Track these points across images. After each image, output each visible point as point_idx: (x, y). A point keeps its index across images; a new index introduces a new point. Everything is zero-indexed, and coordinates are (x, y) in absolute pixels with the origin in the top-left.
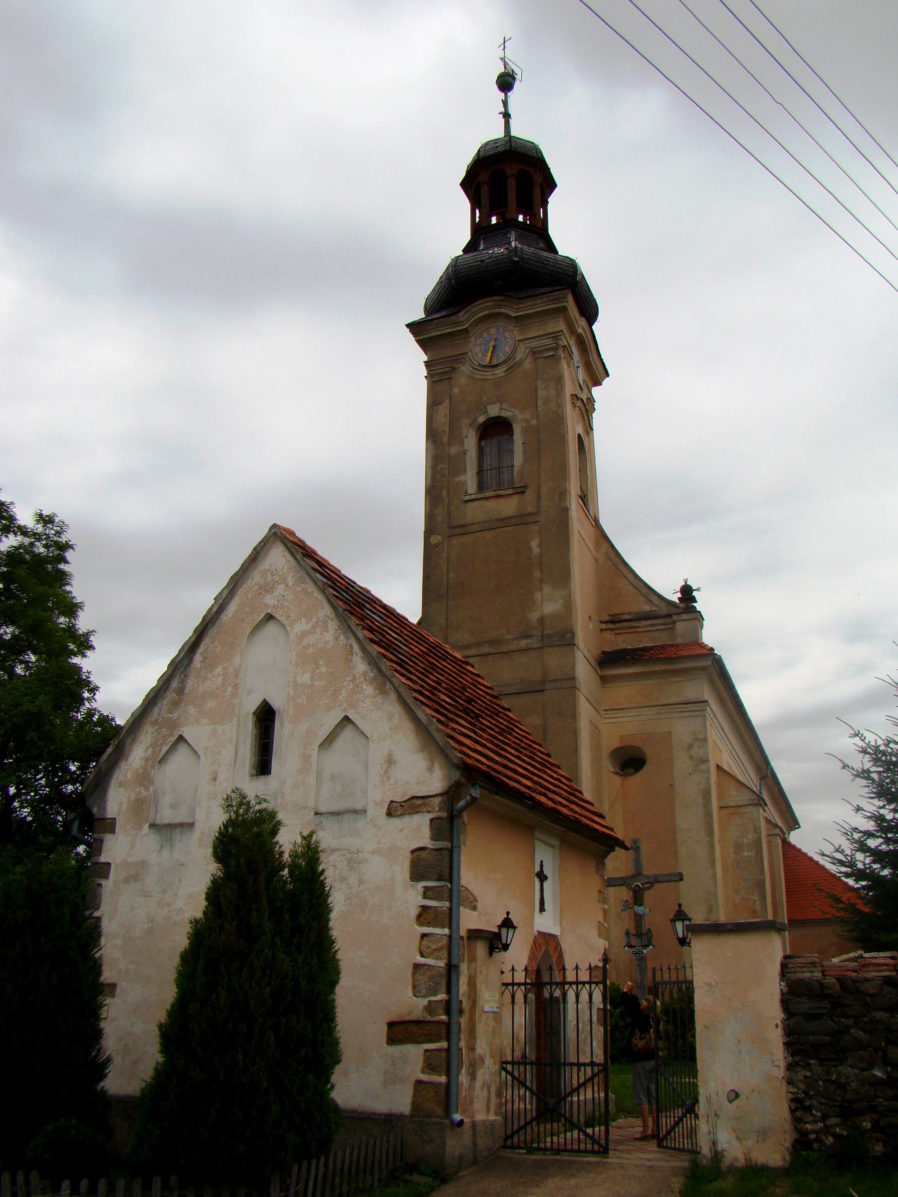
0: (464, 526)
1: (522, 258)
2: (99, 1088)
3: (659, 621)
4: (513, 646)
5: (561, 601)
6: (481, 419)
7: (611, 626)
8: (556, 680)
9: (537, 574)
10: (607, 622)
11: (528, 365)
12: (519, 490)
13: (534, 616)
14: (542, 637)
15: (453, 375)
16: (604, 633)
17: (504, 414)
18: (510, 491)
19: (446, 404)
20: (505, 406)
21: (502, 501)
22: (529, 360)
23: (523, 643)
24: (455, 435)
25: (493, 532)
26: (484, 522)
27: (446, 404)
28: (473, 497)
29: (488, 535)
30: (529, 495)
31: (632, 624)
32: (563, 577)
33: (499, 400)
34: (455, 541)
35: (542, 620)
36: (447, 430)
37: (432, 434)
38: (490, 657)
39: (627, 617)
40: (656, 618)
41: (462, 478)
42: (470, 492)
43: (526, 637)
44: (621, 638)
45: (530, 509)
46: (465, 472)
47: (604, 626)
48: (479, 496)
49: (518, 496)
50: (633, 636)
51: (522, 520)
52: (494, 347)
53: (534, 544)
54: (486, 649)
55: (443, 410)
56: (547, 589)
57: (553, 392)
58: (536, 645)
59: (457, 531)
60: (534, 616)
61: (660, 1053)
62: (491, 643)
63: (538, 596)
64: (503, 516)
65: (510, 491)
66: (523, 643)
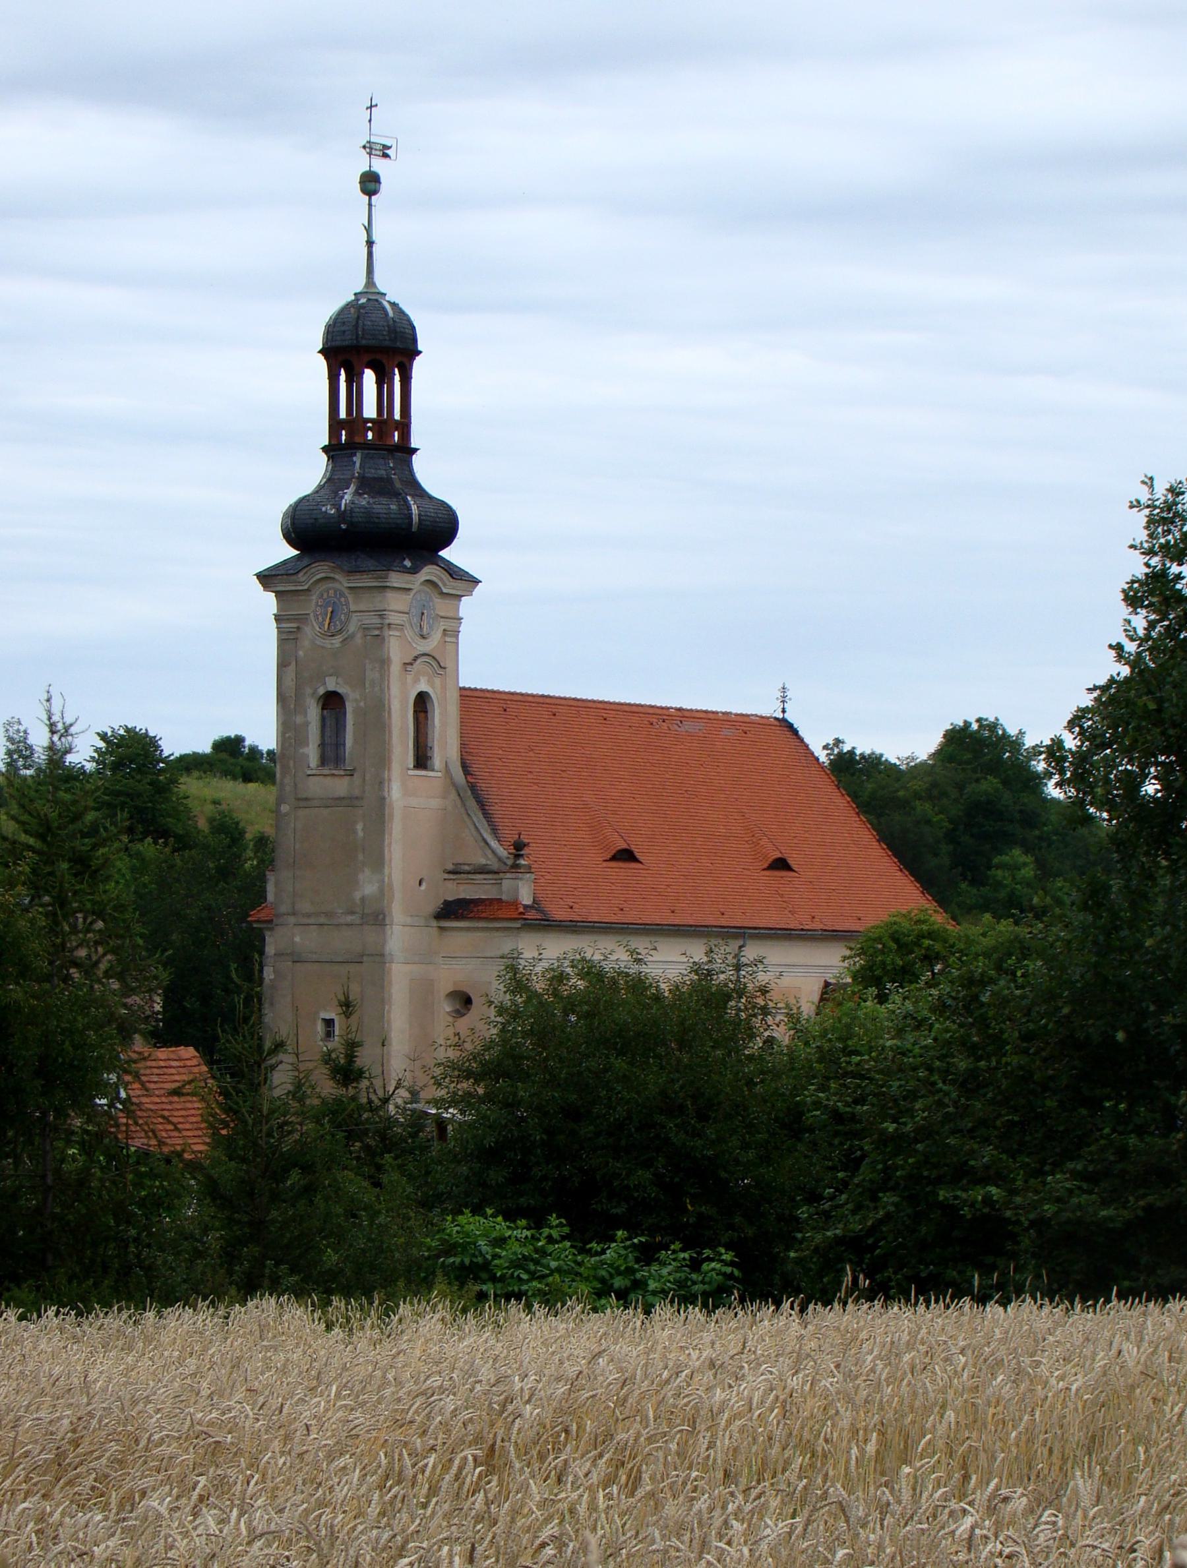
0: (306, 799)
1: (351, 524)
2: (247, 750)
3: (490, 876)
4: (342, 921)
5: (377, 885)
6: (321, 691)
7: (452, 876)
8: (372, 955)
9: (361, 857)
10: (450, 872)
11: (358, 639)
12: (348, 773)
13: (357, 895)
14: (363, 915)
15: (299, 636)
16: (446, 882)
17: (340, 691)
18: (342, 773)
19: (293, 666)
20: (340, 680)
21: (337, 781)
22: (359, 635)
23: (349, 919)
24: (300, 708)
25: (329, 810)
26: (322, 799)
27: (293, 666)
28: (314, 772)
29: (326, 812)
30: (357, 778)
31: (470, 876)
32: (378, 862)
33: (336, 674)
34: (301, 813)
35: (363, 899)
36: (293, 695)
37: (281, 698)
38: (326, 927)
39: (467, 868)
40: (487, 873)
41: (305, 750)
42: (311, 765)
43: (353, 913)
44: (462, 887)
45: (357, 792)
46: (308, 745)
47: (447, 876)
48: (318, 772)
49: (348, 778)
50: (470, 886)
51: (350, 801)
52: (332, 612)
53: (359, 827)
54: (322, 920)
55: (291, 670)
56: (367, 872)
57: (377, 675)
58: (358, 922)
59: (302, 804)
60: (357, 895)
61: (373, 1236)
62: (328, 914)
63: (361, 877)
64: (337, 795)
65: (342, 773)
66: (349, 919)
